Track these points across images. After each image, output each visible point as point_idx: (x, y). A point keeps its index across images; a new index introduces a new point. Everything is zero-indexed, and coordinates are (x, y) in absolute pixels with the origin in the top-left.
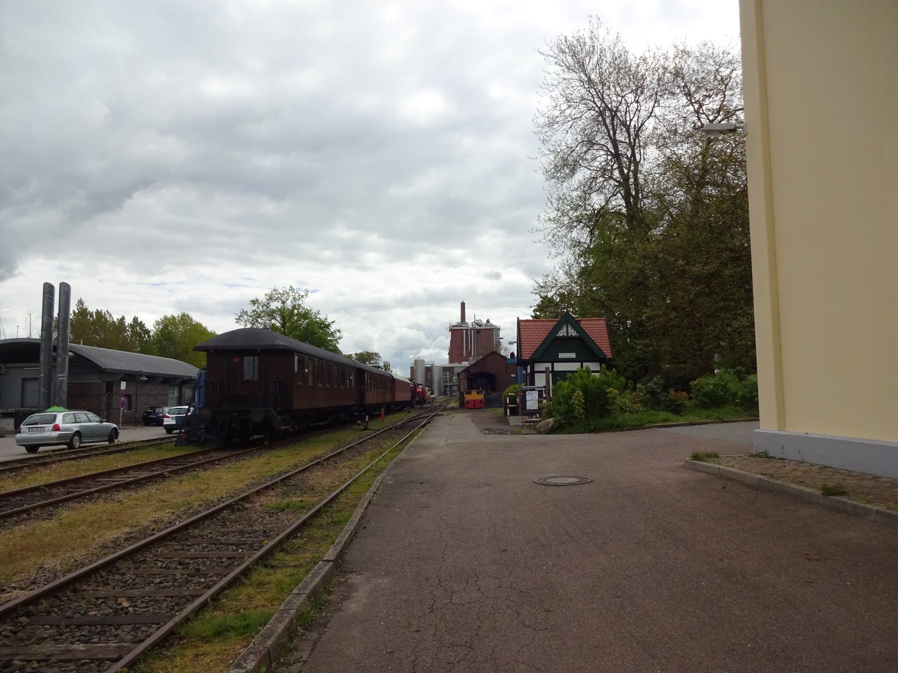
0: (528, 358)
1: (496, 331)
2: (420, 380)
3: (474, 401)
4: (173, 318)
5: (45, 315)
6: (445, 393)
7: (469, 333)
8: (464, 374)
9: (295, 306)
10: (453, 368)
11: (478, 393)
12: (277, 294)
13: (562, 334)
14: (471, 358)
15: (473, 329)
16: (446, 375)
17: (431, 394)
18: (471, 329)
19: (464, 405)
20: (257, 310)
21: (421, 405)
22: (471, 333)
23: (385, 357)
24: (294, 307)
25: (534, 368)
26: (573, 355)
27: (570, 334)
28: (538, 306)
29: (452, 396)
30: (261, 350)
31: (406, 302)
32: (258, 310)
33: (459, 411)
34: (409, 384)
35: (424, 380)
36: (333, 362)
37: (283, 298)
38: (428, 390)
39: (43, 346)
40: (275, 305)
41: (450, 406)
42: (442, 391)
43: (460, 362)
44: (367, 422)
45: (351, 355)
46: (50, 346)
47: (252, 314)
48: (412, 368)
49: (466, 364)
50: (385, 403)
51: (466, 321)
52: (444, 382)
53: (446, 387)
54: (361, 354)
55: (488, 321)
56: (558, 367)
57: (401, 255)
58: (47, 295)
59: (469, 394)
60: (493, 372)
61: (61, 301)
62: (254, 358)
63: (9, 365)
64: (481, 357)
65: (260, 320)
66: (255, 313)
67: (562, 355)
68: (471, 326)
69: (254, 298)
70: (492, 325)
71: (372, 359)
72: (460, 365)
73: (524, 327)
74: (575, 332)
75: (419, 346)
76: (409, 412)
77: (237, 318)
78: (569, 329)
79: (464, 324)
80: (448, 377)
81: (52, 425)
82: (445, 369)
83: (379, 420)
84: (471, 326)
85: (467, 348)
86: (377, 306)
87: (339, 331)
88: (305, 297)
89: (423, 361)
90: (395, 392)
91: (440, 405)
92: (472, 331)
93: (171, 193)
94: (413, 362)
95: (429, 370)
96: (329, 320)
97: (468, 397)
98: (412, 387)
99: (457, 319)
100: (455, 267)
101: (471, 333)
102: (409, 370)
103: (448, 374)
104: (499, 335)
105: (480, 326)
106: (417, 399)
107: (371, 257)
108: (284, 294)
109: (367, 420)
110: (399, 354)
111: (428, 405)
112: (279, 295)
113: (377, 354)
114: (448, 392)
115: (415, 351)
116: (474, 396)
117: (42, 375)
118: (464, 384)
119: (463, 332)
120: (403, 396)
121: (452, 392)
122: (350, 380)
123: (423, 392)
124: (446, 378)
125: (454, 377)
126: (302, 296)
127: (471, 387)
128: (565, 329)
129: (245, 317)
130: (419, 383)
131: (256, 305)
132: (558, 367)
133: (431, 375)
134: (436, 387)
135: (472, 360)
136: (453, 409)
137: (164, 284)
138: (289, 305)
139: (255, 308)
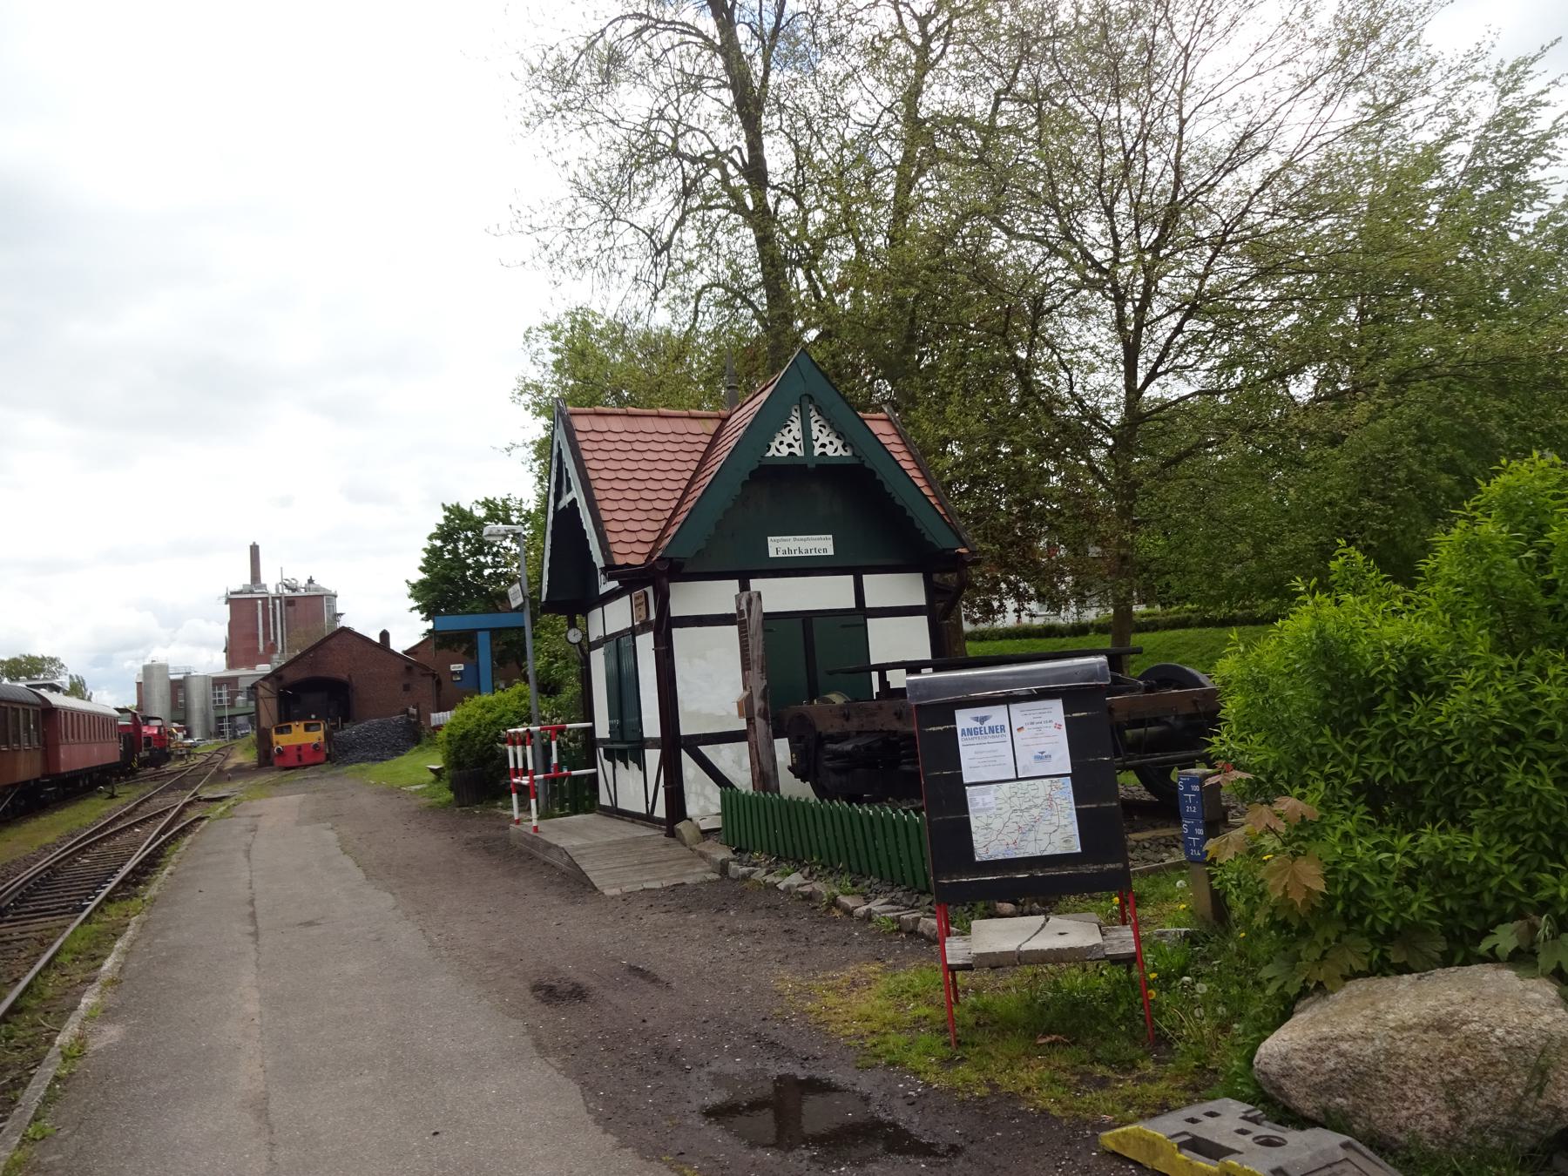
0: (641, 560)
2: (159, 706)
3: (299, 748)
5: (771, 773)
6: (219, 733)
8: (268, 685)
10: (236, 679)
11: (307, 728)
13: (785, 451)
14: (275, 657)
15: (280, 598)
16: (220, 695)
17: (187, 736)
18: (274, 598)
19: (268, 759)
21: (158, 767)
22: (274, 605)
23: (74, 665)
25: (755, 577)
26: (822, 545)
27: (817, 451)
29: (235, 737)
33: (264, 778)
34: (116, 719)
41: (231, 763)
42: (213, 729)
43: (251, 664)
48: (139, 684)
49: (264, 669)
50: (14, 786)
51: (263, 581)
52: (217, 708)
53: (220, 719)
55: (311, 581)
56: (779, 595)
60: (344, 677)
64: (298, 652)
67: (780, 546)
71: (39, 671)
72: (251, 672)
73: (592, 436)
74: (838, 443)
76: (113, 797)
78: (815, 427)
79: (260, 587)
80: (225, 698)
82: (218, 682)
85: (267, 636)
89: (164, 668)
90: (57, 745)
95: (179, 687)
97: (281, 741)
99: (240, 579)
101: (274, 605)
102: (134, 692)
104: (334, 607)
105: (294, 590)
106: (144, 754)
110: (103, 658)
111: (178, 765)
113: (53, 661)
114: (226, 730)
115: (141, 652)
116: (299, 736)
118: (269, 711)
119: (256, 605)
120: (74, 756)
121: (234, 728)
123: (163, 737)
124: (221, 701)
125: (240, 698)
127: (285, 720)
128: (796, 426)
130: (156, 715)
132: (779, 595)
133: (186, 697)
134: (196, 721)
135: (278, 660)
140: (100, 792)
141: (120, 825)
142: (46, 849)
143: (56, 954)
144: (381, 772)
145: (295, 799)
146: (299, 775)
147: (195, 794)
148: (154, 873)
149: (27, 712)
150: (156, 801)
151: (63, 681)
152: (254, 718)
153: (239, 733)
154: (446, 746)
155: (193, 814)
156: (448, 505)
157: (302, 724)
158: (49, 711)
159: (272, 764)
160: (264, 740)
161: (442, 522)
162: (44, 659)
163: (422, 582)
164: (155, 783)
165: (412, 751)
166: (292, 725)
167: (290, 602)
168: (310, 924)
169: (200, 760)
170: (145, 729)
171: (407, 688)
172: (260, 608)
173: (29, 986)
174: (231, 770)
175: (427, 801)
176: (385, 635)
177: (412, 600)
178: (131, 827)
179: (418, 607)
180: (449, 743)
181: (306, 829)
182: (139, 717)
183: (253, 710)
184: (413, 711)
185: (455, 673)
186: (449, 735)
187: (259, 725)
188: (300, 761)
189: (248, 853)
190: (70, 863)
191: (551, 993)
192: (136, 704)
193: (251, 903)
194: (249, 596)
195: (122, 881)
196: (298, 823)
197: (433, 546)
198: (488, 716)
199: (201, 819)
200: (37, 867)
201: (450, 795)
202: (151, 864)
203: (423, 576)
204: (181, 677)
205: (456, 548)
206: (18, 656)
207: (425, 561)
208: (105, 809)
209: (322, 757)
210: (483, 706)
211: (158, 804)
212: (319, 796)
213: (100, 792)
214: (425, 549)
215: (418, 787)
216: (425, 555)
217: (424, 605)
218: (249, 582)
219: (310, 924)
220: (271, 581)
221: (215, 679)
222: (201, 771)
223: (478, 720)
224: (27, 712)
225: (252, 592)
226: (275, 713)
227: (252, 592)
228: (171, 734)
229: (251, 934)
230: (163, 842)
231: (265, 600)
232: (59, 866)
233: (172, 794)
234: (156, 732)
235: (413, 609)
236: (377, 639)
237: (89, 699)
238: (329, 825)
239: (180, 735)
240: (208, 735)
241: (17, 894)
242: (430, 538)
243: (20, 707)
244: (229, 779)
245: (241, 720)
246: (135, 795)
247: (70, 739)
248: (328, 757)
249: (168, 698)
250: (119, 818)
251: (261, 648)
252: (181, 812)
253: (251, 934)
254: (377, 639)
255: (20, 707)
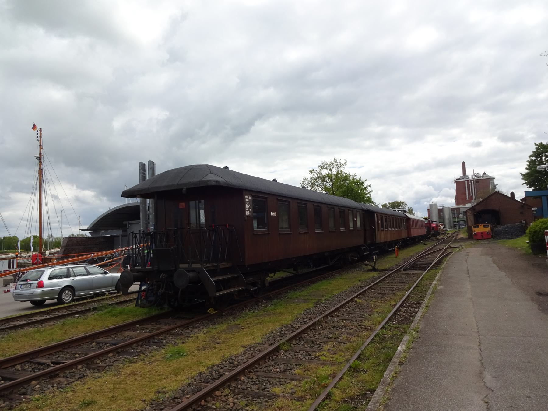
1: (491, 180)
2: (435, 218)
3: (482, 233)
4: (527, 229)
6: (454, 227)
7: (470, 183)
8: (470, 212)
9: (339, 172)
10: (459, 208)
11: (484, 227)
12: (326, 165)
14: (473, 201)
15: (473, 180)
16: (454, 214)
17: (444, 227)
18: (471, 180)
19: (471, 236)
20: (314, 177)
21: (436, 237)
22: (471, 183)
23: (410, 204)
24: (338, 172)
28: (534, 152)
29: (460, 228)
30: (188, 189)
31: (420, 168)
32: (314, 177)
33: (470, 242)
34: (424, 222)
35: (438, 219)
36: (347, 207)
37: (330, 167)
38: (442, 225)
39: (141, 208)
40: (325, 172)
42: (452, 226)
44: (375, 262)
45: (386, 204)
46: (146, 207)
47: (311, 179)
48: (428, 210)
49: (469, 205)
50: (401, 239)
51: (467, 175)
52: (453, 218)
53: (455, 222)
54: (393, 203)
55: (484, 174)
57: (415, 138)
58: (141, 171)
59: (476, 228)
60: (497, 209)
61: (149, 174)
62: (196, 203)
63: (131, 222)
64: (481, 200)
65: (316, 183)
66: (313, 179)
68: (471, 178)
69: (311, 169)
70: (487, 176)
71: (400, 206)
75: (431, 196)
76: (425, 244)
77: (302, 183)
80: (456, 215)
81: (37, 282)
82: (453, 210)
83: (393, 256)
84: (471, 178)
85: (469, 194)
86: (401, 173)
87: (370, 186)
88: (345, 165)
89: (436, 205)
90: (410, 229)
91: (451, 236)
92: (473, 182)
93: (276, 120)
94: (429, 206)
95: (441, 211)
96: (363, 180)
97: (475, 230)
98: (428, 224)
99: (459, 174)
100: (454, 141)
101: (471, 183)
102: (427, 212)
103: (456, 213)
104: (494, 183)
105: (478, 177)
106: (432, 232)
107: (395, 142)
108: (330, 165)
109: (374, 260)
110: (418, 201)
111: (442, 237)
112: (327, 166)
113: (403, 203)
115: (429, 199)
116: (481, 229)
117: (142, 228)
119: (465, 183)
120: (416, 232)
121: (459, 225)
122: (355, 223)
123: (437, 227)
124: (454, 216)
126: (343, 164)
127: (477, 223)
129: (307, 182)
131: (313, 174)
133: (443, 214)
134: (447, 222)
135: (474, 203)
136: (462, 239)
137: (276, 171)
138: (334, 172)
139: (312, 176)
140: (421, 243)
141: (429, 252)
142: (412, 257)
143: (422, 278)
144: (510, 243)
145: (480, 249)
146: (482, 242)
147: (449, 245)
148: (441, 264)
149: (403, 219)
150: (437, 247)
151: (406, 209)
152: (466, 222)
153: (461, 227)
154: (529, 235)
155: (449, 251)
156: (537, 143)
157: (483, 225)
158: (408, 219)
159: (473, 238)
160: (470, 230)
161: (535, 150)
162: (401, 202)
163: (527, 174)
164: (436, 242)
165: (523, 236)
166: (479, 225)
167: (477, 181)
168: (483, 276)
169: (449, 235)
170: (432, 225)
171: (522, 213)
172: (466, 184)
173: (418, 283)
174: (459, 239)
175: (524, 252)
176: (513, 194)
177: (523, 180)
178: (432, 253)
179: (525, 183)
180: (530, 234)
181: (483, 257)
182: (429, 219)
183: (465, 219)
184: (524, 222)
185: (533, 211)
186: (530, 231)
187: (468, 224)
188: (482, 237)
189: (466, 261)
190: (419, 260)
191: (540, 294)
192: (428, 216)
193: (468, 271)
194: (462, 180)
195: (433, 265)
196: (481, 255)
197: (531, 159)
198: (544, 226)
199: (452, 252)
200: (412, 260)
201: (531, 251)
202: (439, 263)
203: (527, 171)
204: (441, 208)
205: (541, 159)
206: (393, 201)
207: (528, 165)
208: (424, 248)
209: (490, 236)
210: (542, 222)
211: (439, 247)
212: (488, 248)
213: (421, 243)
214: (528, 161)
215: (522, 248)
216: (528, 163)
217: (528, 182)
218: (462, 175)
219: (483, 276)
220: (470, 174)
221: (452, 208)
222: (450, 239)
223: (540, 227)
224: (403, 219)
225: (463, 179)
226: (473, 221)
227: (463, 179)
228: (439, 227)
229: (468, 276)
230: (442, 257)
231: (468, 181)
232: (416, 261)
233: (442, 245)
234: (435, 226)
235: (524, 184)
236: (509, 196)
237: (414, 215)
238: (490, 256)
239: (442, 227)
240: (451, 227)
241: (409, 266)
242: (530, 157)
243: (402, 218)
244: (459, 242)
245: (461, 223)
246: (431, 244)
247: (414, 227)
248: (492, 237)
249: (437, 215)
250: (428, 250)
251: (467, 198)
252: (446, 250)
253: (468, 276)
254: (509, 196)
255: (402, 218)
